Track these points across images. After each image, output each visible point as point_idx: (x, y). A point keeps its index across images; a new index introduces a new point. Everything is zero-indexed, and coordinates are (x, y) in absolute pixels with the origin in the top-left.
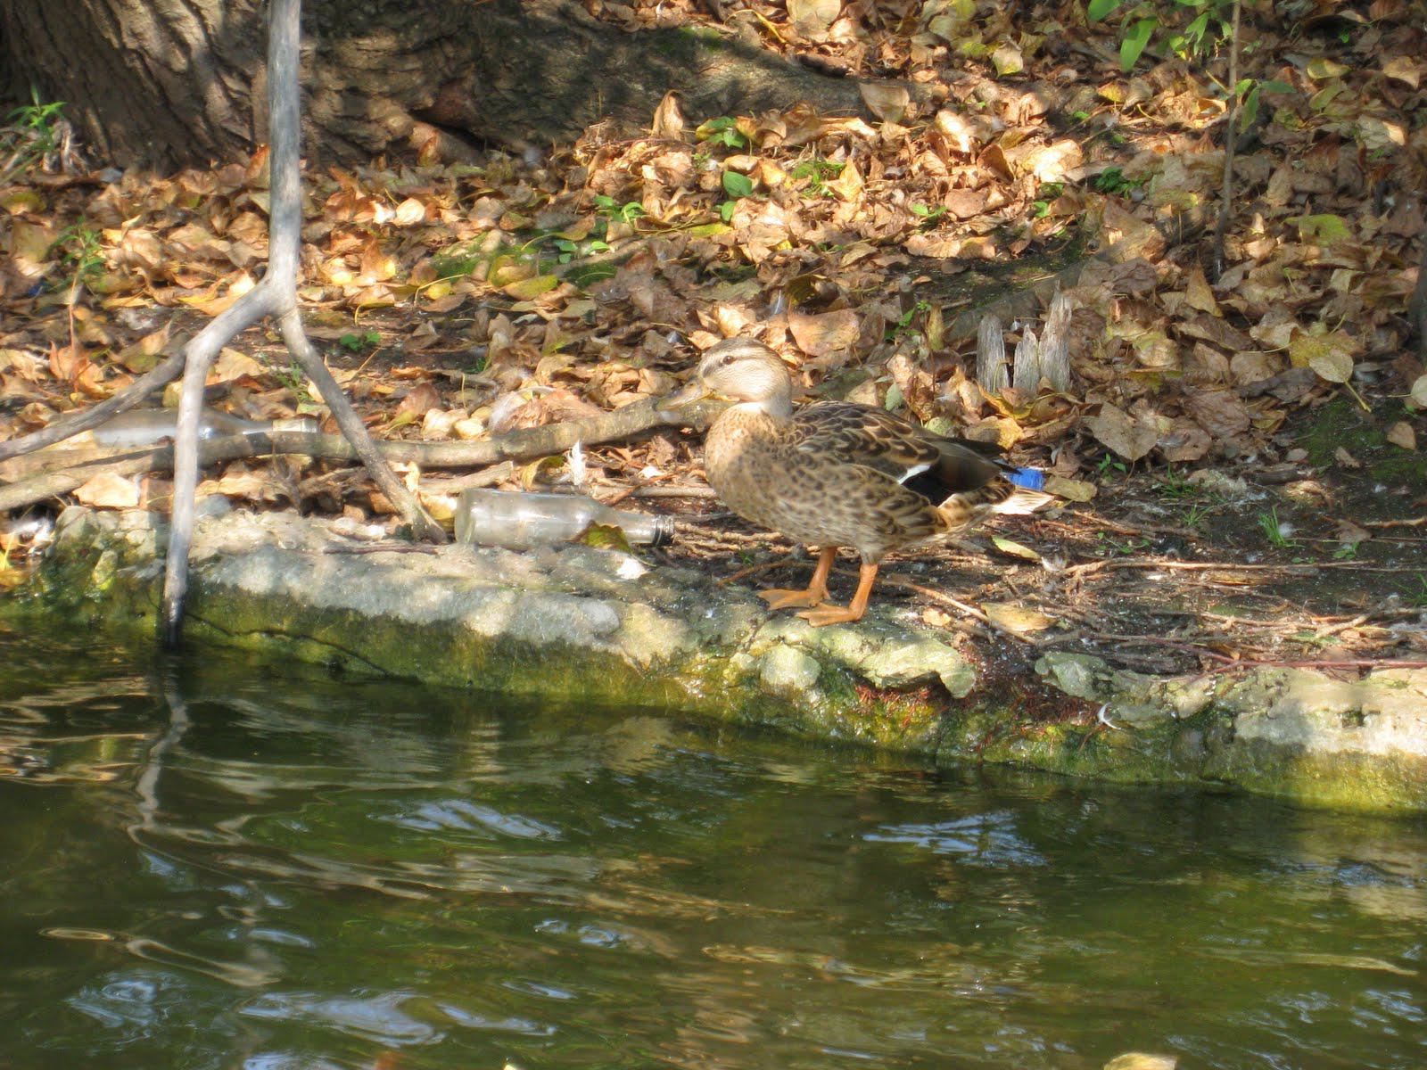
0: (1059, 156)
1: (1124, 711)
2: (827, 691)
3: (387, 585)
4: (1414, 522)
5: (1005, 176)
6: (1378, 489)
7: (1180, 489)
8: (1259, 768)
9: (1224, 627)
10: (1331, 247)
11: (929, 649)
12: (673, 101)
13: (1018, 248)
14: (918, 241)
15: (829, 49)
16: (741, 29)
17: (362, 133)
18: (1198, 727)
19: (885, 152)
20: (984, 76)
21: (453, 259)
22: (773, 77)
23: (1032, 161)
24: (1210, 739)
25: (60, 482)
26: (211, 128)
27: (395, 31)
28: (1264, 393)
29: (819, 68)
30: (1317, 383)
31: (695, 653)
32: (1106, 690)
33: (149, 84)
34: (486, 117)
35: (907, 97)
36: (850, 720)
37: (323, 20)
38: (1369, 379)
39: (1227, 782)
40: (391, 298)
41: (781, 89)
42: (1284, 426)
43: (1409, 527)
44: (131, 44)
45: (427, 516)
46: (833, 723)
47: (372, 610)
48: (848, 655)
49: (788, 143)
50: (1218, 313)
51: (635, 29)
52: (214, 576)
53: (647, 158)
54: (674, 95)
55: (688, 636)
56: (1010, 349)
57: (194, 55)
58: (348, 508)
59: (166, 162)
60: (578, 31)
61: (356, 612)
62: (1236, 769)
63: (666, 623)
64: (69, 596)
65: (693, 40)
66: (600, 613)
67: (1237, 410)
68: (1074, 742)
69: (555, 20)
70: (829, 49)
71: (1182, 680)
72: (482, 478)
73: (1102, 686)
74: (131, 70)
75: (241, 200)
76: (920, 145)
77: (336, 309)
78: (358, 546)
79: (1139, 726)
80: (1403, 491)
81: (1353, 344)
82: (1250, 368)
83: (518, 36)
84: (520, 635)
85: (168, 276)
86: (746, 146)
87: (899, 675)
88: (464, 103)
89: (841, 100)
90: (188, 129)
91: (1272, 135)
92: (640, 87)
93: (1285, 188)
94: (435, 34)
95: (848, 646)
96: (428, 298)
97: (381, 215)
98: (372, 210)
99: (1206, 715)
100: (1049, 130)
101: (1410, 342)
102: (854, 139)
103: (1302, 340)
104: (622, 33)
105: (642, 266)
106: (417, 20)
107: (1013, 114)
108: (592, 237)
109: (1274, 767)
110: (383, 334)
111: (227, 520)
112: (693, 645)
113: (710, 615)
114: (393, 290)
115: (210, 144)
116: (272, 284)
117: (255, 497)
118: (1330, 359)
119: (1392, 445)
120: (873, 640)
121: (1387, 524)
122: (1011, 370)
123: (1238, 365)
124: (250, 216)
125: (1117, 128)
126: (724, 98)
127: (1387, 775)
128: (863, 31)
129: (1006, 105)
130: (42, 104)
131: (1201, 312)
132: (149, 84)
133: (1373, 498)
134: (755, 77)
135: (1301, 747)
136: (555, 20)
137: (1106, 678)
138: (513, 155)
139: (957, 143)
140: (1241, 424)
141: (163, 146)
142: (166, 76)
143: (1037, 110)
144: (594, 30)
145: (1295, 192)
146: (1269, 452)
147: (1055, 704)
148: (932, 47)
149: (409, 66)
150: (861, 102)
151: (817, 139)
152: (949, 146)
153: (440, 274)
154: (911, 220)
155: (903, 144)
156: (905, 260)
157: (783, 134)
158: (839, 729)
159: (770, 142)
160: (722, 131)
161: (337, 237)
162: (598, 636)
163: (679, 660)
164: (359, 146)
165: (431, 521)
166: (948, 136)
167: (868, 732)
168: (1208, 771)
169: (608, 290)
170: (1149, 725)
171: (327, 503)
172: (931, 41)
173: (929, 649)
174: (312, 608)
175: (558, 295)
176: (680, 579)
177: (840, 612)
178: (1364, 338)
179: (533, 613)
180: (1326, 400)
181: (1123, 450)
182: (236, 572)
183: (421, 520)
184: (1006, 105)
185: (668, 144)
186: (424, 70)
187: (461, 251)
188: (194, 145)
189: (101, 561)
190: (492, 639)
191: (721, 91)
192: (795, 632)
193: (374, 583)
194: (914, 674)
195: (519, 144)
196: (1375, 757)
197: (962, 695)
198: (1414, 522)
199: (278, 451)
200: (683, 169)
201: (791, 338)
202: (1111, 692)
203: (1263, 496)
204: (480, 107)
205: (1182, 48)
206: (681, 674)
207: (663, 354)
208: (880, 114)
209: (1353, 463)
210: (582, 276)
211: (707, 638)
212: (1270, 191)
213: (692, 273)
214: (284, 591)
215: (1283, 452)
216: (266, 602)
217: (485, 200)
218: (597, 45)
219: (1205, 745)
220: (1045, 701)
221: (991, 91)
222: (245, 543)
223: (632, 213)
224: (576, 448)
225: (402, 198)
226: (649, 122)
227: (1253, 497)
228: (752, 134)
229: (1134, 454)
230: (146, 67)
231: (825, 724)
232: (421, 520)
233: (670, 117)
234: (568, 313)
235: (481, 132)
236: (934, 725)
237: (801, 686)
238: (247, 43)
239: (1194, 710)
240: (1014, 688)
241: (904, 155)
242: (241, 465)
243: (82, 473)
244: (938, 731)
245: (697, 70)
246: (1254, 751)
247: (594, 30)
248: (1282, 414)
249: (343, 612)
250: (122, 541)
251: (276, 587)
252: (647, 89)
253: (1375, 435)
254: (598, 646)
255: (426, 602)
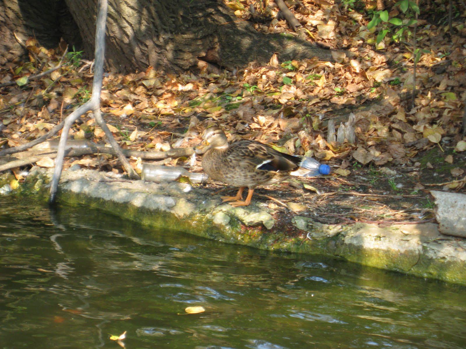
0: (384, 74)
1: (314, 235)
2: (232, 226)
3: (112, 191)
4: (440, 184)
5: (366, 80)
6: (435, 175)
7: (375, 173)
8: (350, 252)
9: (360, 212)
10: (448, 102)
11: (264, 216)
12: (276, 55)
13: (363, 101)
14: (335, 99)
15: (327, 41)
16: (300, 34)
17: (182, 63)
18: (334, 240)
19: (334, 72)
20: (372, 50)
21: (196, 101)
22: (307, 49)
23: (375, 75)
24: (337, 243)
25: (33, 159)
26: (137, 61)
27: (195, 33)
28: (412, 145)
29: (321, 46)
30: (429, 143)
31: (197, 214)
32: (310, 228)
33: (117, 47)
34: (223, 60)
35: (345, 56)
36: (237, 235)
37: (171, 29)
38: (447, 142)
39: (341, 256)
40: (173, 112)
41: (309, 53)
42: (416, 155)
43: (438, 186)
44: (112, 35)
45: (134, 172)
46: (232, 236)
47: (107, 199)
48: (239, 216)
49: (307, 69)
50: (405, 121)
51: (268, 33)
52: (65, 187)
53: (265, 73)
54: (276, 54)
55: (195, 209)
56: (336, 130)
57: (130, 38)
58: (114, 169)
59: (125, 71)
60: (250, 34)
61: (103, 199)
62: (344, 253)
63: (189, 205)
64: (27, 192)
65: (283, 37)
66: (170, 201)
67: (402, 150)
68: (298, 243)
69: (244, 30)
70: (327, 41)
71: (333, 226)
72: (161, 163)
73: (310, 227)
74: (113, 43)
75: (140, 83)
76: (345, 70)
77: (154, 115)
78: (111, 180)
79: (318, 239)
80: (442, 176)
81: (443, 132)
82: (409, 138)
83: (233, 35)
84: (147, 206)
85: (108, 104)
86: (295, 70)
87: (251, 222)
88: (216, 54)
89: (327, 56)
90: (130, 61)
91: (450, 69)
92: (267, 51)
93: (445, 84)
94: (207, 34)
95: (240, 213)
96: (185, 113)
97: (180, 88)
98: (178, 86)
99: (338, 235)
100: (386, 66)
101: (461, 131)
102: (326, 68)
103: (427, 129)
104: (264, 34)
105: (249, 104)
106: (201, 29)
107: (376, 61)
108: (239, 95)
109: (354, 252)
110: (165, 123)
111: (76, 171)
112: (197, 211)
113: (203, 203)
114: (173, 110)
115: (137, 66)
116: (92, 101)
117: (87, 165)
118: (434, 135)
119: (446, 162)
120: (248, 211)
121: (432, 185)
122: (336, 136)
123: (406, 137)
124: (141, 87)
125: (405, 66)
126: (291, 55)
127: (386, 256)
128: (339, 36)
129: (374, 59)
130: (76, 51)
131: (400, 121)
132: (117, 47)
133: (433, 178)
134: (301, 49)
135: (362, 246)
136: (244, 30)
137: (311, 224)
138: (230, 71)
139: (355, 70)
140: (403, 155)
141: (124, 66)
142: (123, 45)
143: (384, 61)
144: (255, 34)
145: (448, 86)
146: (409, 163)
147: (294, 232)
148: (359, 41)
149: (198, 43)
150: (332, 57)
151: (316, 68)
152: (353, 70)
153: (190, 105)
154: (334, 93)
155: (340, 70)
156: (327, 104)
157: (306, 66)
158: (234, 238)
159: (301, 69)
160: (288, 65)
161: (165, 94)
162: (169, 208)
163: (192, 215)
164: (181, 68)
165: (135, 174)
166: (353, 67)
167: (243, 239)
168: (336, 253)
169: (234, 111)
170: (321, 239)
171: (108, 168)
172: (359, 39)
173: (264, 216)
174: (91, 197)
175: (220, 112)
176: (201, 192)
177: (242, 203)
178: (446, 130)
179: (151, 201)
180: (432, 148)
181: (361, 161)
182: (70, 186)
183: (132, 173)
184: (374, 59)
185: (272, 68)
186: (203, 45)
187: (199, 99)
188: (133, 66)
189: (38, 182)
190: (139, 208)
191: (290, 53)
192: (225, 208)
193: (108, 190)
194: (256, 222)
195: (232, 68)
196: (383, 250)
197: (270, 228)
198: (440, 184)
199: (100, 152)
200: (273, 76)
201: (279, 126)
202: (312, 229)
203: (401, 176)
204: (220, 56)
205: (396, 39)
206: (191, 220)
207: (241, 130)
208: (336, 60)
209: (432, 167)
210: (229, 108)
211: (201, 210)
212: (440, 86)
213: (263, 107)
214: (83, 192)
215: (413, 163)
216: (78, 195)
217: (212, 84)
218: (256, 38)
219: (336, 245)
220: (293, 231)
221: (372, 54)
222: (81, 180)
223: (254, 89)
224: (194, 155)
225: (188, 83)
226: (268, 61)
227: (397, 176)
228: (297, 66)
229: (365, 162)
230: (116, 42)
231: (230, 236)
232: (132, 173)
233: (274, 61)
234: (221, 117)
235: (221, 64)
236: (260, 237)
237: (224, 224)
238: (147, 35)
239: (334, 235)
240: (286, 227)
241: (340, 73)
242: (89, 156)
243: (39, 157)
244: (261, 239)
245: (284, 46)
246: (349, 247)
247: (255, 34)
248: (416, 152)
249: (99, 199)
250: (45, 177)
251: (81, 191)
252: (269, 52)
253: (442, 159)
254: (168, 211)
255: (120, 196)
